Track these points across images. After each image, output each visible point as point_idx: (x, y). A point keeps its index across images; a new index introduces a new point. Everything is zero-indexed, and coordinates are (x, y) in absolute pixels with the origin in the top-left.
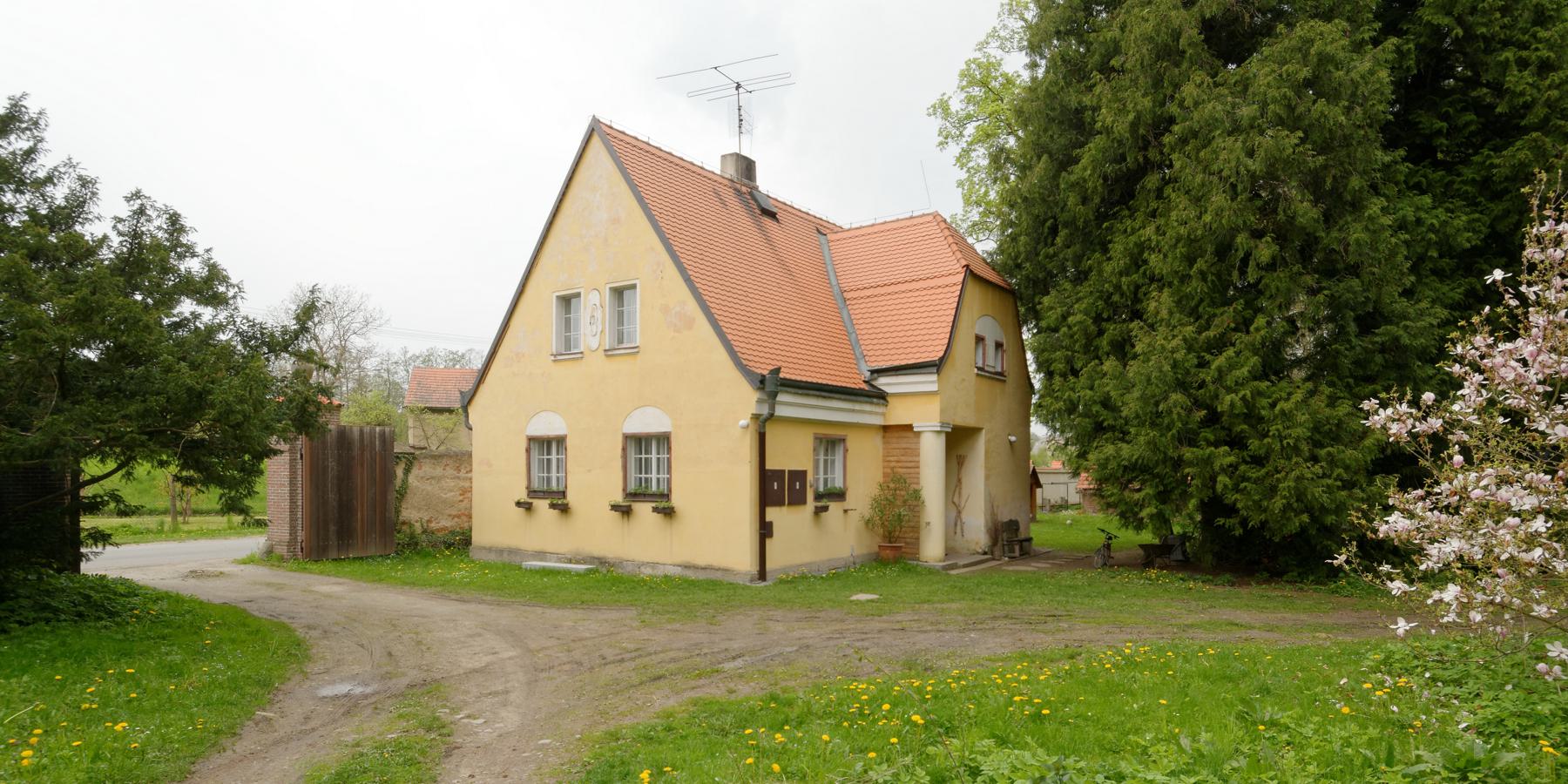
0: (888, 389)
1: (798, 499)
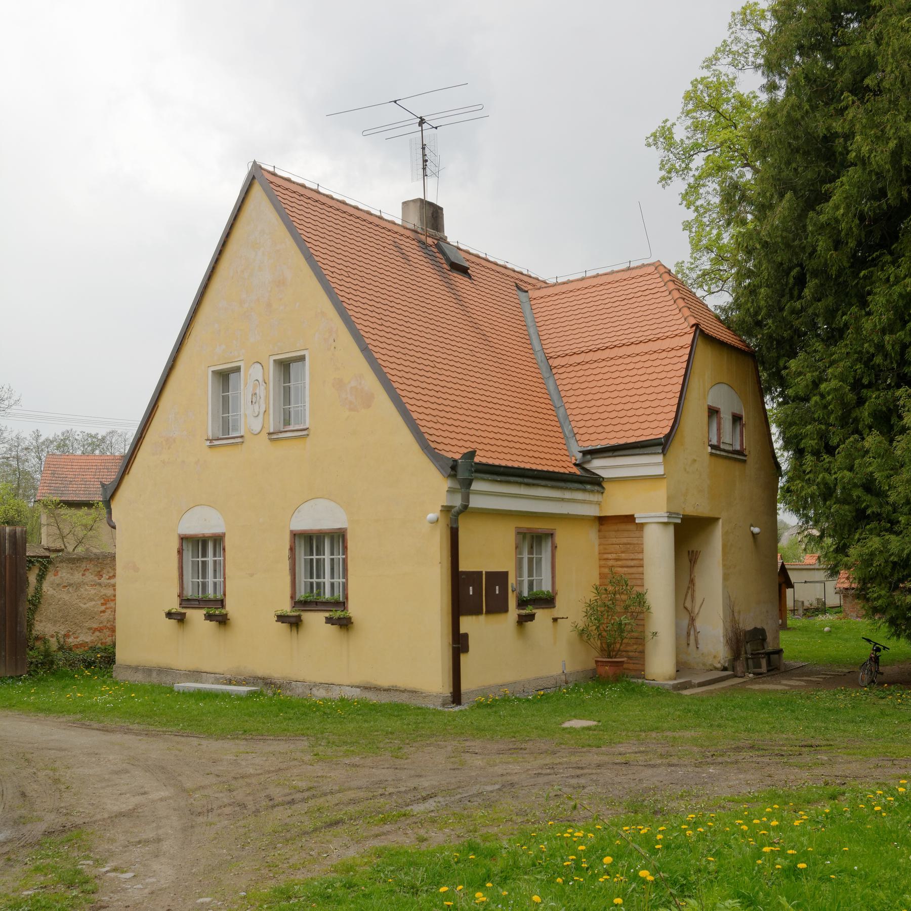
0: (604, 474)
1: (498, 607)
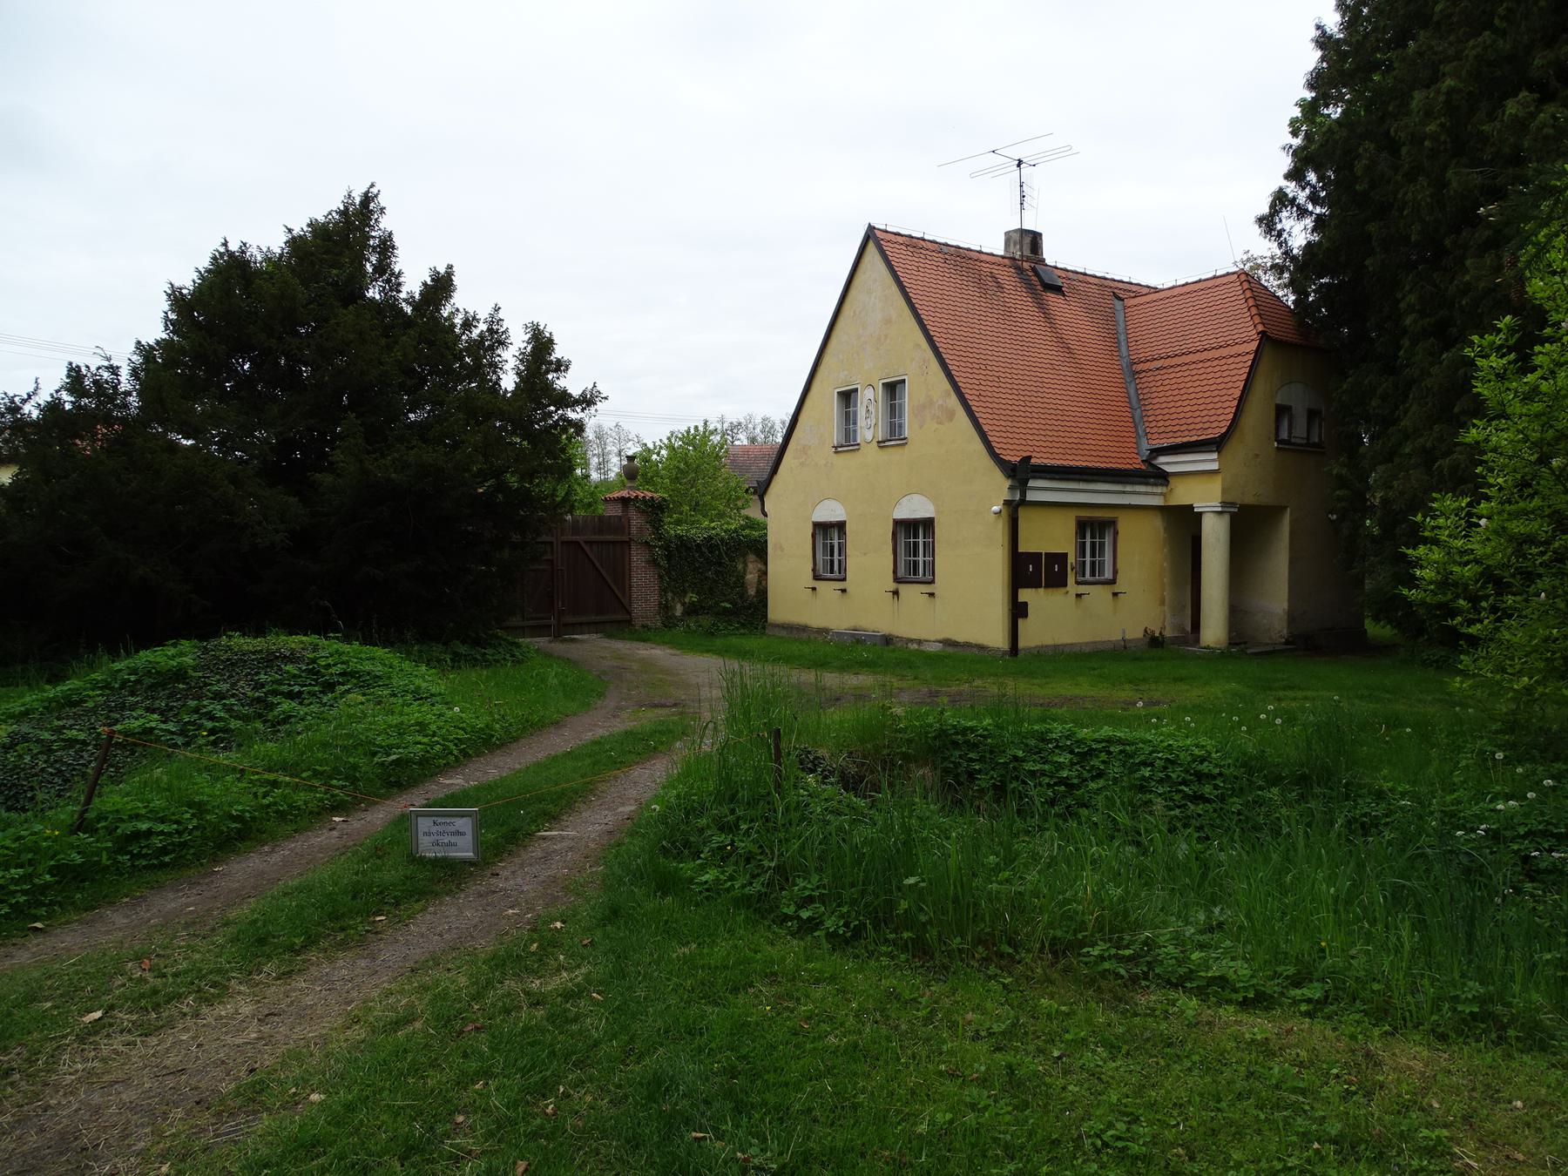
0: (1168, 469)
1: (1057, 581)
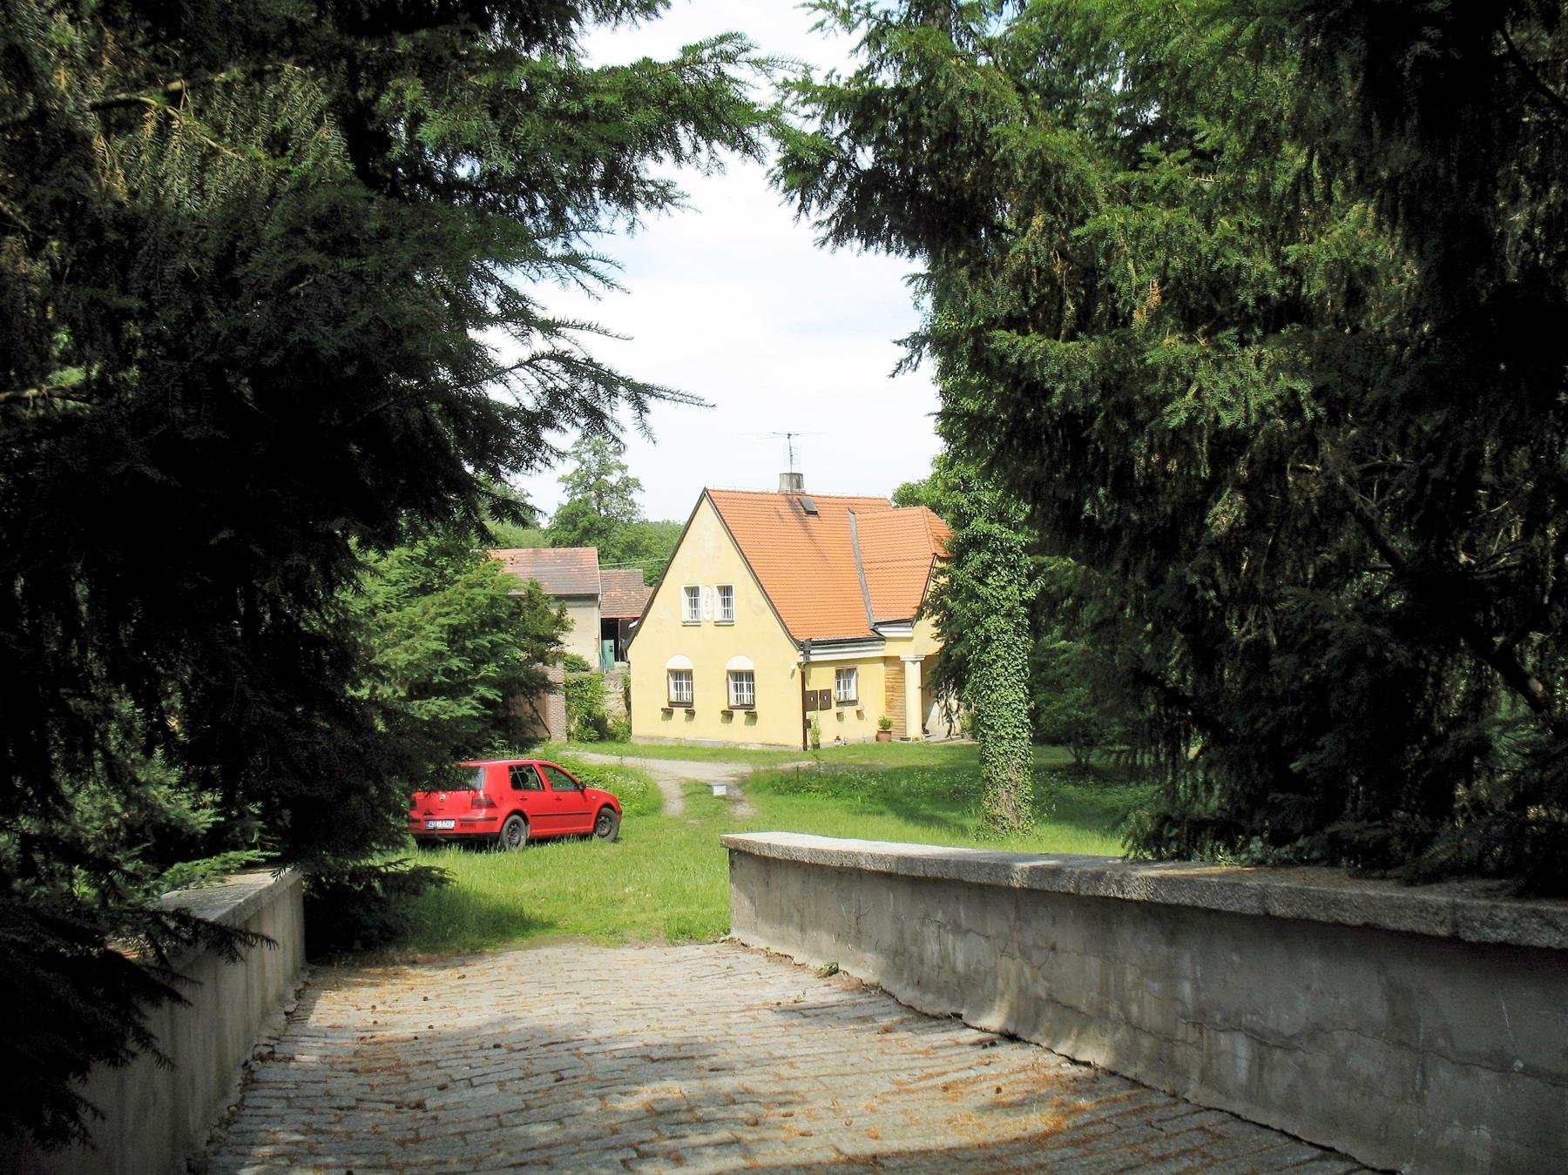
1: (826, 706)
